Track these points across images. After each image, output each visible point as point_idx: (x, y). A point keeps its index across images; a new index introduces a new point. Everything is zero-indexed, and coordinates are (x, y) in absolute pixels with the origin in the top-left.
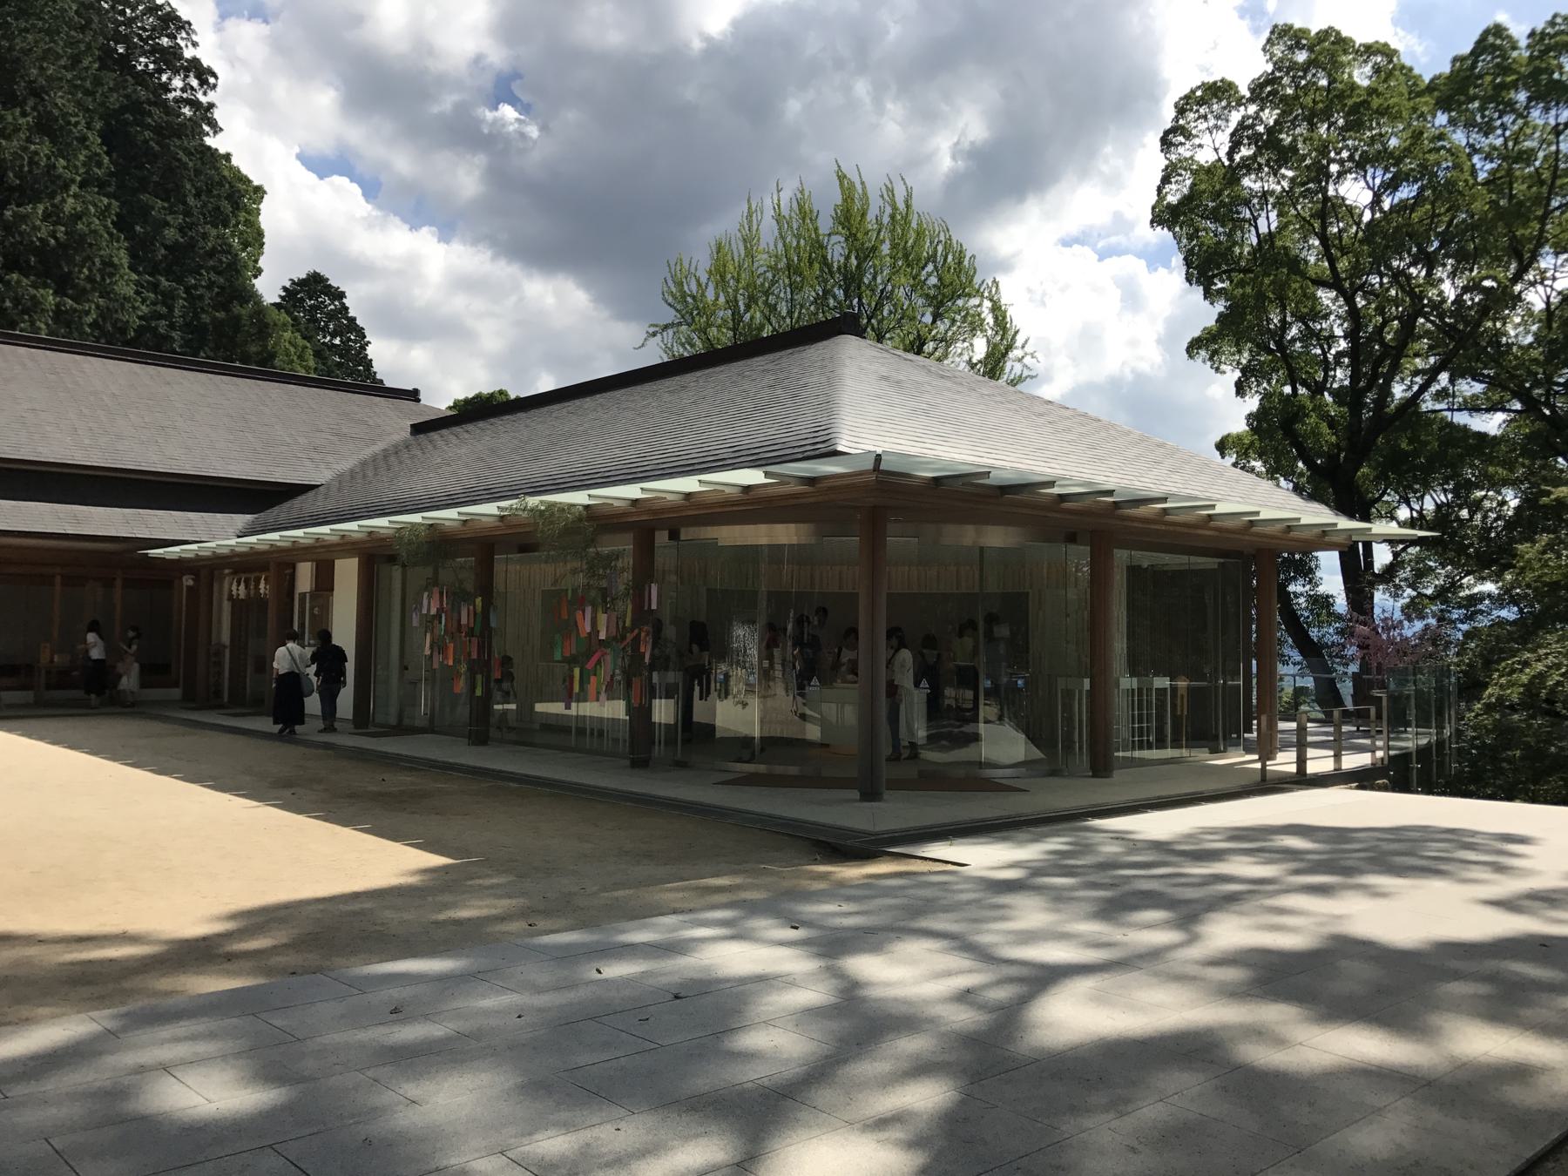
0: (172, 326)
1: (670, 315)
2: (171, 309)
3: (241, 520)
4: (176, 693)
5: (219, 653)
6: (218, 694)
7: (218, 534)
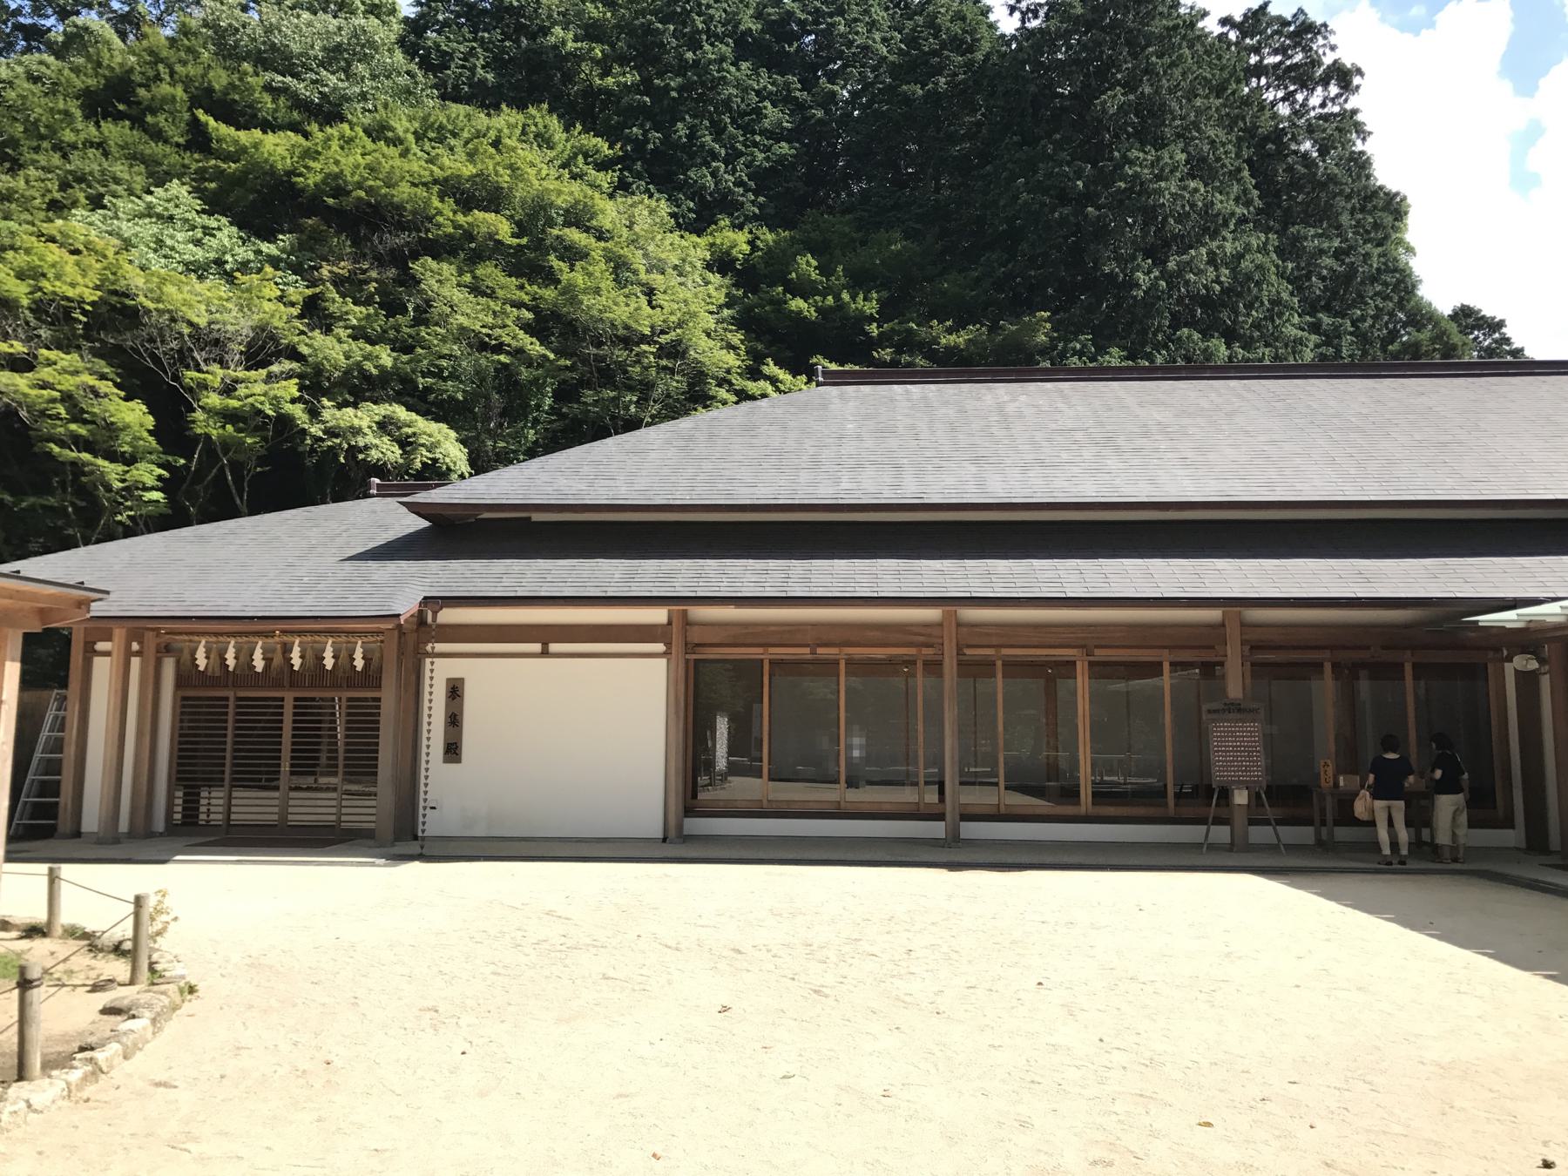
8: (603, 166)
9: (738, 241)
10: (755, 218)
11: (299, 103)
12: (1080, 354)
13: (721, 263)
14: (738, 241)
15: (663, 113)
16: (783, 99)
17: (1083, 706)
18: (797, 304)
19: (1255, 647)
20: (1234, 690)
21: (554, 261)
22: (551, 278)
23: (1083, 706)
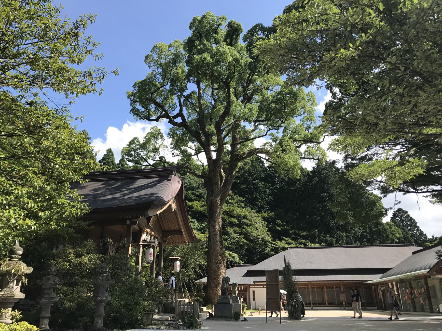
0: (367, 233)
1: (435, 237)
2: (366, 230)
3: (380, 275)
4: (376, 308)
5: (381, 300)
6: (382, 307)
7: (376, 278)
8: (242, 202)
9: (265, 215)
10: (268, 210)
11: (196, 195)
12: (323, 236)
13: (264, 219)
14: (265, 215)
15: (251, 193)
16: (269, 188)
17: (326, 293)
18: (278, 228)
19: (344, 285)
20: (342, 290)
21: (245, 227)
22: (244, 228)
23: (326, 293)
